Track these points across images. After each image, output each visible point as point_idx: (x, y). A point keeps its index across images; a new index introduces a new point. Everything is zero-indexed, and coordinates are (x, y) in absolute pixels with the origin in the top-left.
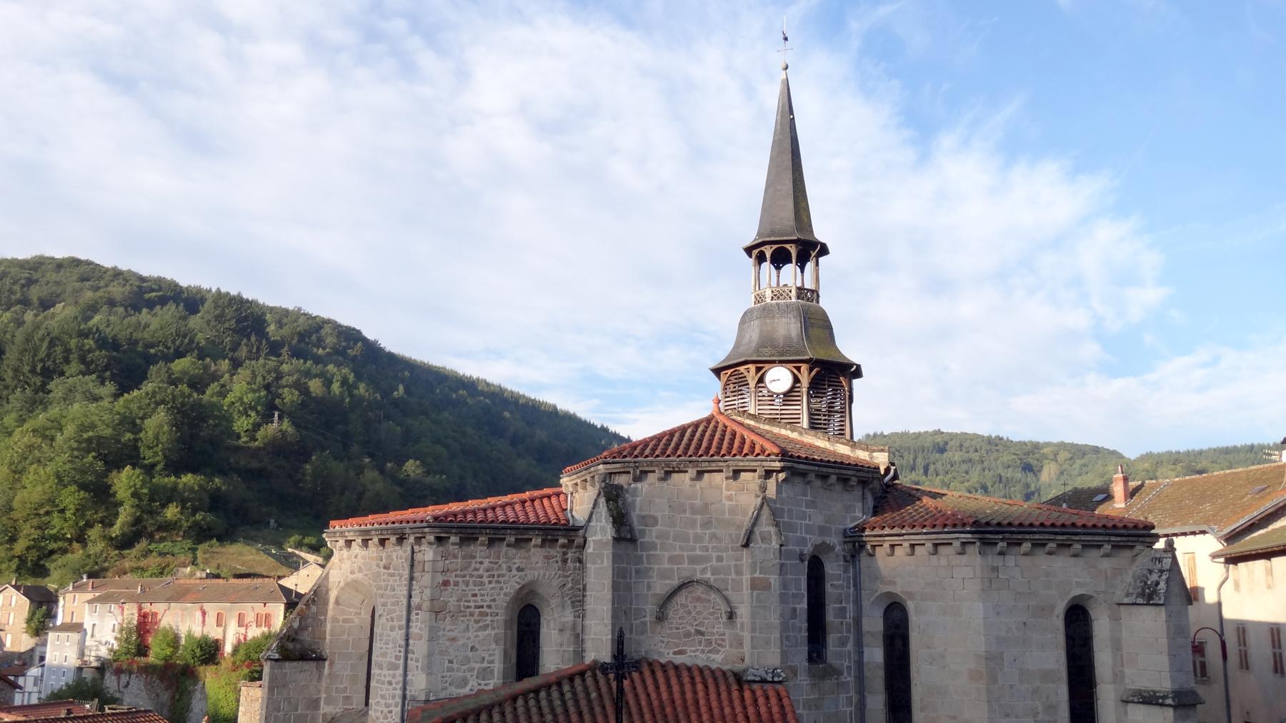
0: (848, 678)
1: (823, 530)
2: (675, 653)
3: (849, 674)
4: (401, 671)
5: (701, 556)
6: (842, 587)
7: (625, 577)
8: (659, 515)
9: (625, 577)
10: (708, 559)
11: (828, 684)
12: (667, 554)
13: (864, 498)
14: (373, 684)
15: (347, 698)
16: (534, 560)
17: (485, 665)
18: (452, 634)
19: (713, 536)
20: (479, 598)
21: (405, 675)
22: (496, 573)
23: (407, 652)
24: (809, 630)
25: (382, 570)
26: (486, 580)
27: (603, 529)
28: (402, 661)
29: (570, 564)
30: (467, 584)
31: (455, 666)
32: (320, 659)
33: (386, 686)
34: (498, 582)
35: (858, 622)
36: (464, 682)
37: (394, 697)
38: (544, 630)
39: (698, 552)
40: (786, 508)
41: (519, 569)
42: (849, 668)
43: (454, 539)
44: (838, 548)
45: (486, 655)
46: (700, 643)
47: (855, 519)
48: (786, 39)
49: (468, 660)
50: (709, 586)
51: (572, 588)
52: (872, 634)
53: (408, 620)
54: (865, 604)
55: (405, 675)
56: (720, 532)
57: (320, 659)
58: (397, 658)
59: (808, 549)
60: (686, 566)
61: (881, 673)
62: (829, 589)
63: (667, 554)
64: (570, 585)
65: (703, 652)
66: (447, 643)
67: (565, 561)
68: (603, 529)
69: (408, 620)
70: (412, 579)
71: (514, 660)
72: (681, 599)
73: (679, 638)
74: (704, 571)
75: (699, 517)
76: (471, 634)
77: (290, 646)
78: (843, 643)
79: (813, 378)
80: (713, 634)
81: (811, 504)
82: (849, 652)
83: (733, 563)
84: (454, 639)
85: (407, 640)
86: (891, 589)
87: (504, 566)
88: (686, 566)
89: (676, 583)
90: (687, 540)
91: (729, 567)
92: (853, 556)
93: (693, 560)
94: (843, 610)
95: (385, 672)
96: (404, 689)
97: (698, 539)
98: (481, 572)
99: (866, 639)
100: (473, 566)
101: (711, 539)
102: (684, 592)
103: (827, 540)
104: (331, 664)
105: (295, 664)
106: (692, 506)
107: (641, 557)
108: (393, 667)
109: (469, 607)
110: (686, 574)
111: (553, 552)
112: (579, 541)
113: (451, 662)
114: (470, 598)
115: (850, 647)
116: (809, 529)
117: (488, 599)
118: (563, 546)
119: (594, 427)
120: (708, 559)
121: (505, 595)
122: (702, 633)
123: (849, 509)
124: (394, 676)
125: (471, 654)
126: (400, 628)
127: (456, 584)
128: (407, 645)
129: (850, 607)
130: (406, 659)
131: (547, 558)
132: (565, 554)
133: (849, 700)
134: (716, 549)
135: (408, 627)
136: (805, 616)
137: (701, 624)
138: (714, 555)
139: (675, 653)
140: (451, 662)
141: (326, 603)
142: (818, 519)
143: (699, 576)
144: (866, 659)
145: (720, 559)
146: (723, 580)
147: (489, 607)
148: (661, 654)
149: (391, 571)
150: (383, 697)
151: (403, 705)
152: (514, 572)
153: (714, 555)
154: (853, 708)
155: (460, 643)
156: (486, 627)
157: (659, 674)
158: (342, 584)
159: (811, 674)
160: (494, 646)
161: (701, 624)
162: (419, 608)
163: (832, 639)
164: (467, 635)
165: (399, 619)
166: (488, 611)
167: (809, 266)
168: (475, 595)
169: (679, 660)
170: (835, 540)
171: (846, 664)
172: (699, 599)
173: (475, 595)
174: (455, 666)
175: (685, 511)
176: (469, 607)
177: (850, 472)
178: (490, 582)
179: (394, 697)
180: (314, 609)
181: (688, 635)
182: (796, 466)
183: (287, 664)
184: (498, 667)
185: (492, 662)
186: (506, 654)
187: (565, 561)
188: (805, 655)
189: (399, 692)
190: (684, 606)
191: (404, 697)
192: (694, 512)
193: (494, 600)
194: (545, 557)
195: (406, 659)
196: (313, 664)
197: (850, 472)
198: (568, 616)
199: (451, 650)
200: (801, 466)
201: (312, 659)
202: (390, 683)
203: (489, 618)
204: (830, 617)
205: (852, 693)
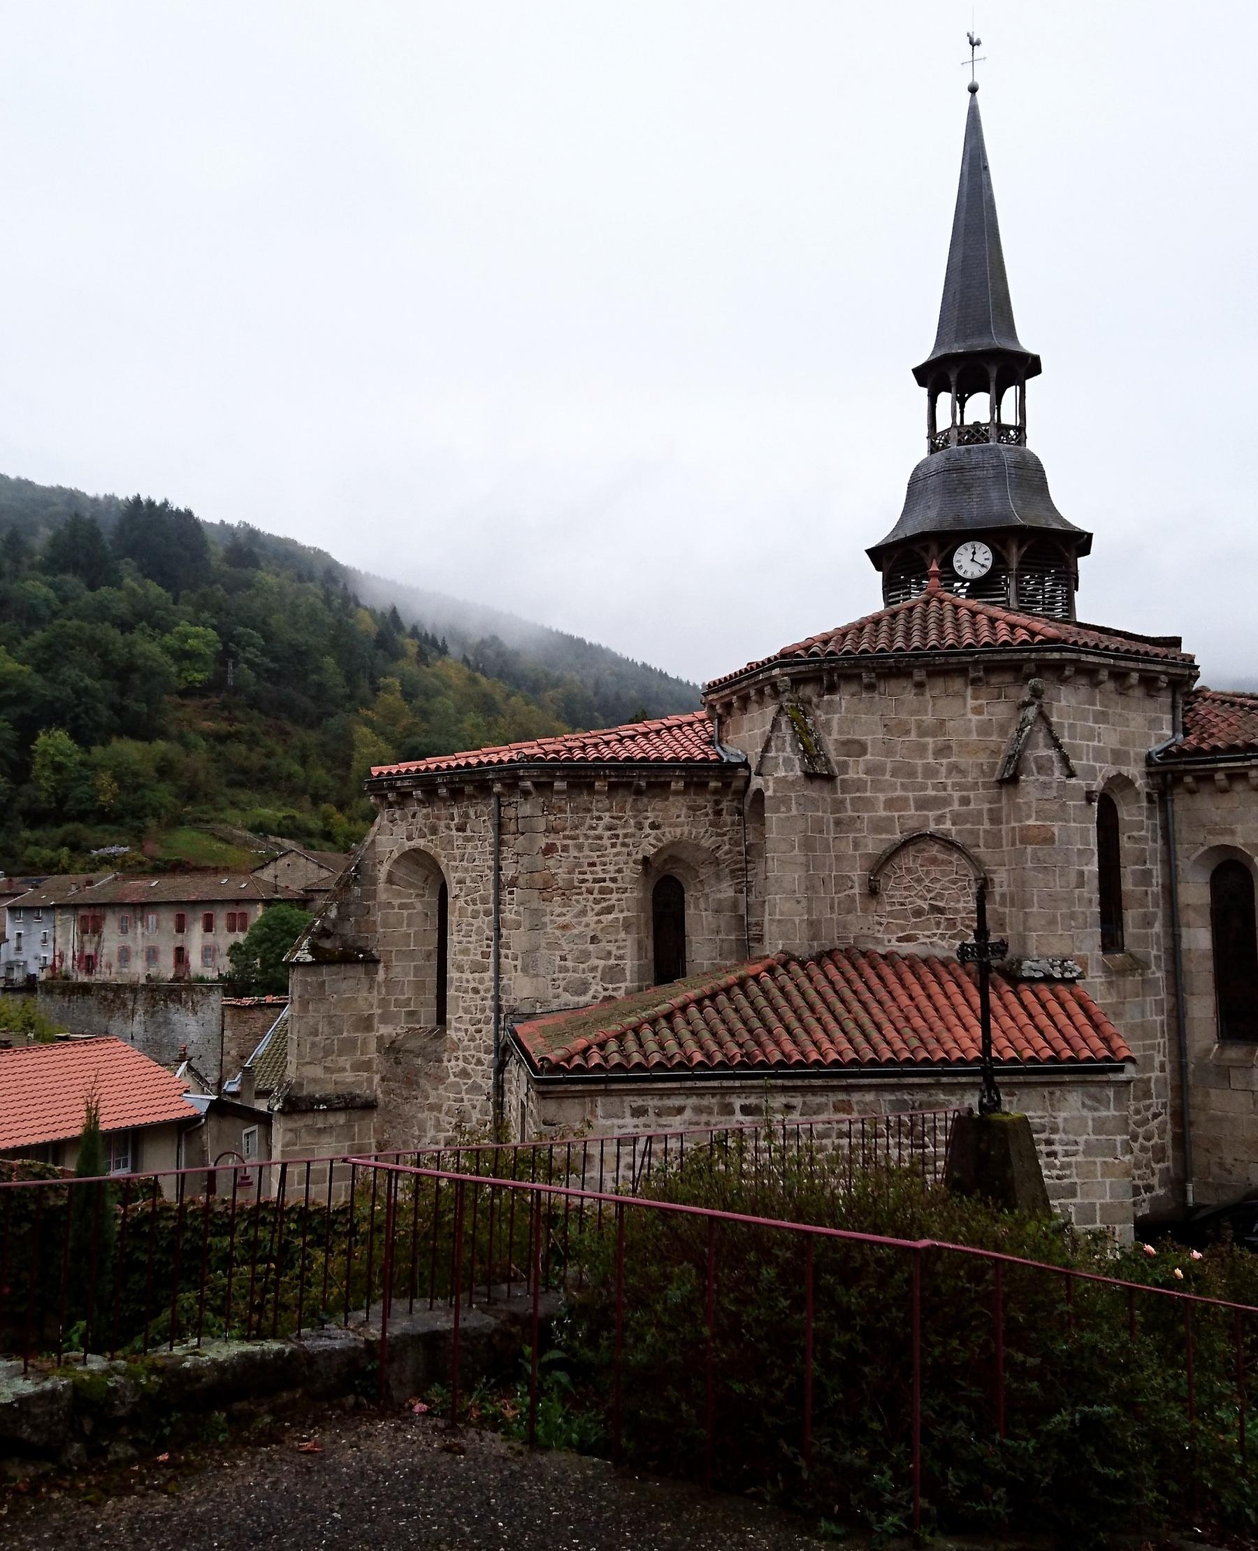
0: (1158, 974)
1: (1119, 756)
2: (900, 940)
3: (1159, 967)
4: (491, 973)
5: (936, 798)
6: (1144, 839)
7: (821, 832)
8: (868, 739)
9: (821, 832)
10: (946, 802)
11: (1132, 981)
12: (882, 797)
13: (1174, 707)
14: (451, 992)
15: (411, 1014)
16: (674, 811)
17: (612, 962)
18: (561, 920)
19: (954, 768)
20: (598, 868)
21: (498, 978)
22: (620, 832)
23: (498, 947)
24: (1102, 904)
25: (454, 832)
26: (606, 842)
27: (788, 761)
28: (492, 960)
29: (726, 818)
30: (580, 848)
31: (569, 964)
32: (371, 962)
33: (471, 995)
34: (624, 845)
35: (1170, 891)
36: (583, 988)
37: (483, 1010)
38: (690, 912)
39: (931, 792)
40: (1066, 722)
41: (654, 826)
42: (1158, 958)
43: (559, 785)
44: (1139, 783)
45: (611, 947)
46: (938, 924)
47: (1160, 739)
48: (974, 43)
49: (585, 956)
50: (949, 844)
51: (730, 852)
52: (1195, 909)
53: (498, 902)
54: (1183, 864)
55: (498, 978)
56: (965, 761)
57: (371, 962)
58: (485, 955)
59: (1097, 785)
60: (913, 812)
61: (1209, 965)
62: (1125, 843)
63: (882, 797)
64: (727, 847)
65: (942, 937)
66: (558, 932)
67: (718, 813)
68: (788, 761)
69: (498, 902)
70: (500, 843)
71: (651, 955)
72: (907, 860)
73: (906, 918)
74: (940, 819)
75: (930, 740)
76: (591, 918)
77: (327, 944)
78: (1147, 922)
79: (1024, 556)
80: (956, 911)
81: (1101, 717)
82: (1158, 935)
83: (986, 806)
84: (565, 927)
85: (498, 929)
86: (1226, 840)
87: (632, 822)
88: (913, 812)
89: (898, 836)
90: (912, 774)
91: (980, 812)
92: (1162, 795)
93: (922, 804)
94: (1146, 877)
95: (467, 975)
96: (497, 998)
97: (930, 772)
98: (599, 831)
99: (1187, 916)
100: (588, 822)
101: (949, 772)
102: (911, 850)
103: (1125, 770)
104: (387, 968)
105: (334, 968)
106: (919, 725)
107: (843, 802)
108: (479, 968)
109: (584, 881)
110: (912, 824)
111: (700, 801)
112: (737, 784)
113: (563, 959)
114: (586, 868)
115: (1158, 928)
116: (1098, 754)
117: (612, 868)
118: (715, 791)
119: (634, 664)
120: (946, 802)
121: (635, 862)
122: (941, 911)
123: (1154, 723)
124: (481, 981)
125: (591, 947)
126: (487, 913)
127: (565, 848)
128: (499, 936)
129: (1157, 870)
130: (498, 956)
131: (693, 809)
132: (717, 803)
133: (1159, 1003)
134: (959, 786)
135: (498, 911)
136: (1096, 883)
137: (940, 896)
138: (956, 795)
139: (900, 940)
140: (563, 959)
141: (374, 881)
142: (1110, 738)
143: (932, 827)
144: (1184, 946)
145: (965, 801)
146: (971, 832)
147: (614, 880)
148: (878, 941)
149: (469, 833)
150: (466, 1011)
151: (498, 1021)
152: (648, 831)
153: (956, 795)
154: (1164, 1017)
155: (576, 931)
156: (609, 910)
157: (887, 971)
158: (396, 855)
159: (1107, 970)
160: (623, 935)
161: (940, 896)
162: (513, 883)
163: (1130, 916)
164: (585, 920)
165: (484, 901)
166: (612, 885)
167: (1010, 394)
168: (593, 864)
169: (907, 948)
170: (1134, 770)
171: (1154, 952)
172: (934, 861)
173: (593, 864)
174: (569, 964)
175: (908, 732)
176: (584, 881)
177: (1159, 668)
178: (614, 845)
179: (483, 1010)
180: (357, 890)
181: (918, 913)
182: (1084, 657)
183: (325, 969)
184: (629, 964)
185: (620, 958)
186: (640, 945)
187: (718, 813)
188: (1098, 940)
189: (490, 1003)
190: (909, 870)
191: (498, 1009)
192: (922, 733)
193: (619, 871)
194: (689, 808)
195: (498, 956)
196: (360, 970)
197: (1159, 668)
198: (726, 891)
199: (562, 942)
200: (1091, 659)
201: (358, 961)
202: (476, 991)
203: (615, 896)
204: (1127, 885)
205: (1163, 995)
